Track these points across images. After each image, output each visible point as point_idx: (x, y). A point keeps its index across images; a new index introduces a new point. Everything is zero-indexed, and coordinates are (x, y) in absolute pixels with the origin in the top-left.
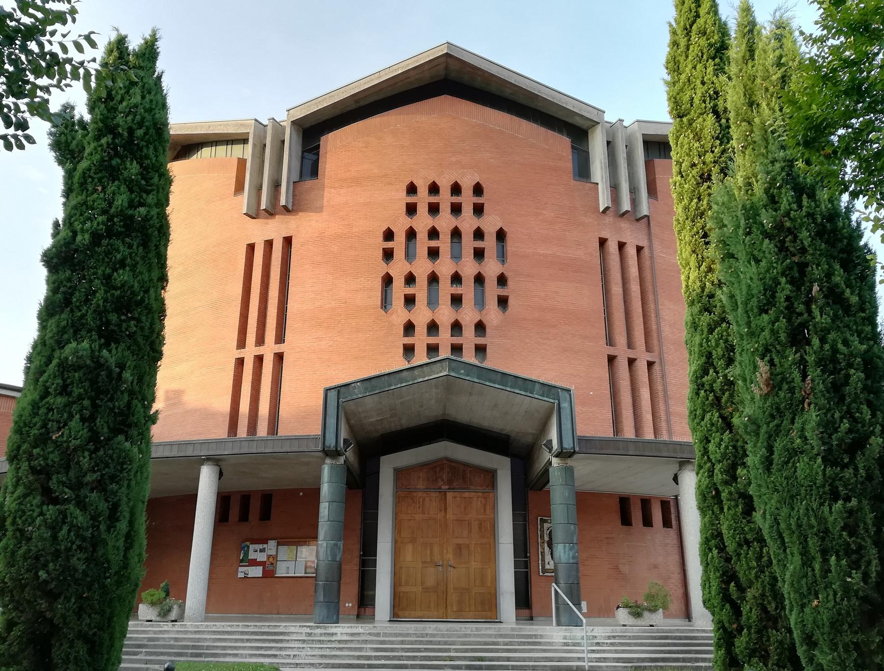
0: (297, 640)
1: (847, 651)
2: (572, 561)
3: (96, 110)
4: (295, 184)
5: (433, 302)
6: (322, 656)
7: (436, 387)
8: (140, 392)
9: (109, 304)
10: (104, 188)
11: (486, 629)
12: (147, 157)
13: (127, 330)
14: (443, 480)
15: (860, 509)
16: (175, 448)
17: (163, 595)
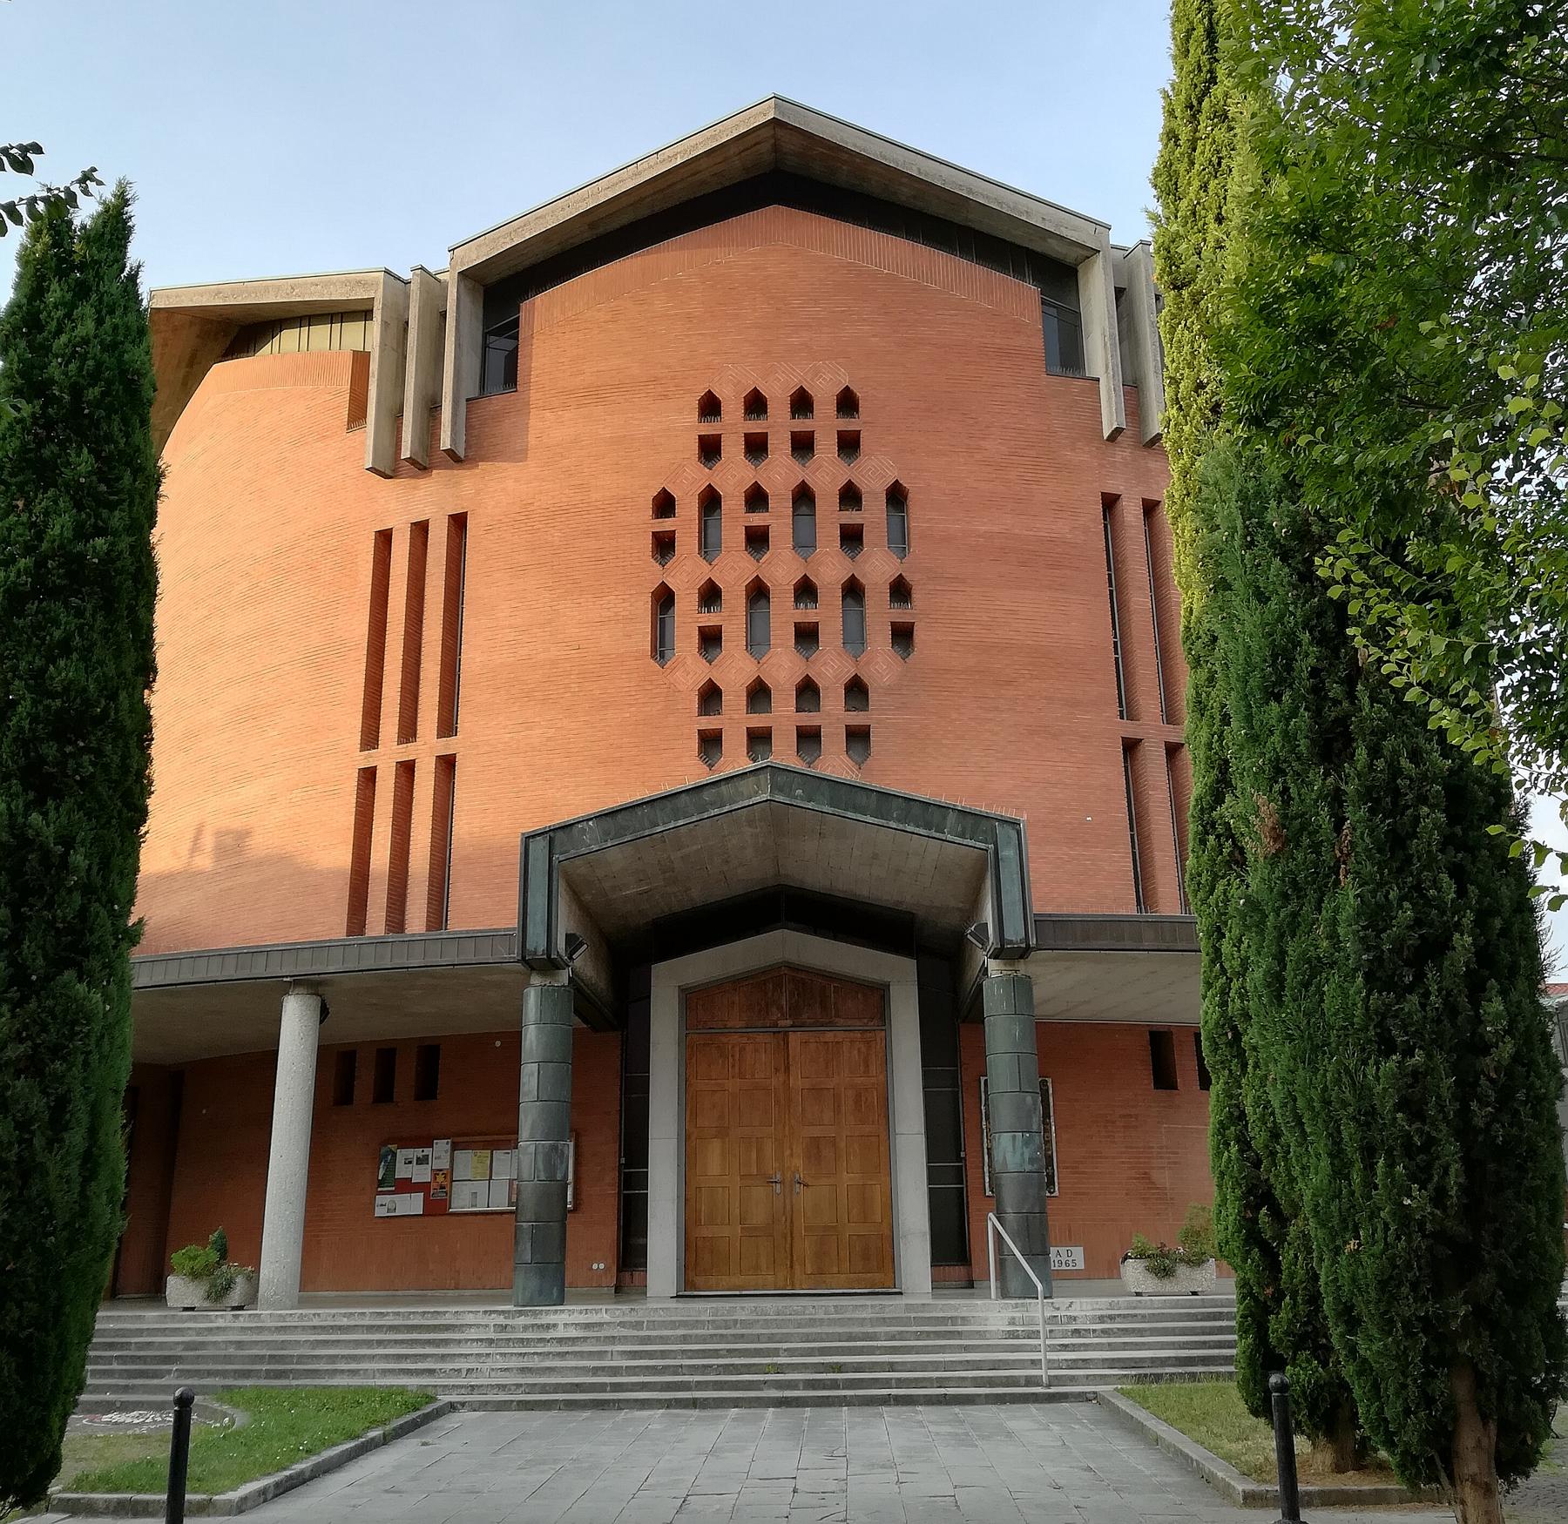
0: (477, 1340)
1: (1409, 1334)
2: (1028, 1167)
3: (11, 352)
4: (470, 405)
5: (756, 642)
6: (523, 1370)
7: (751, 823)
8: (104, 888)
9: (41, 726)
10: (28, 507)
12: (109, 438)
13: (76, 772)
14: (780, 1008)
15: (1430, 1071)
16: (231, 961)
17: (214, 1256)
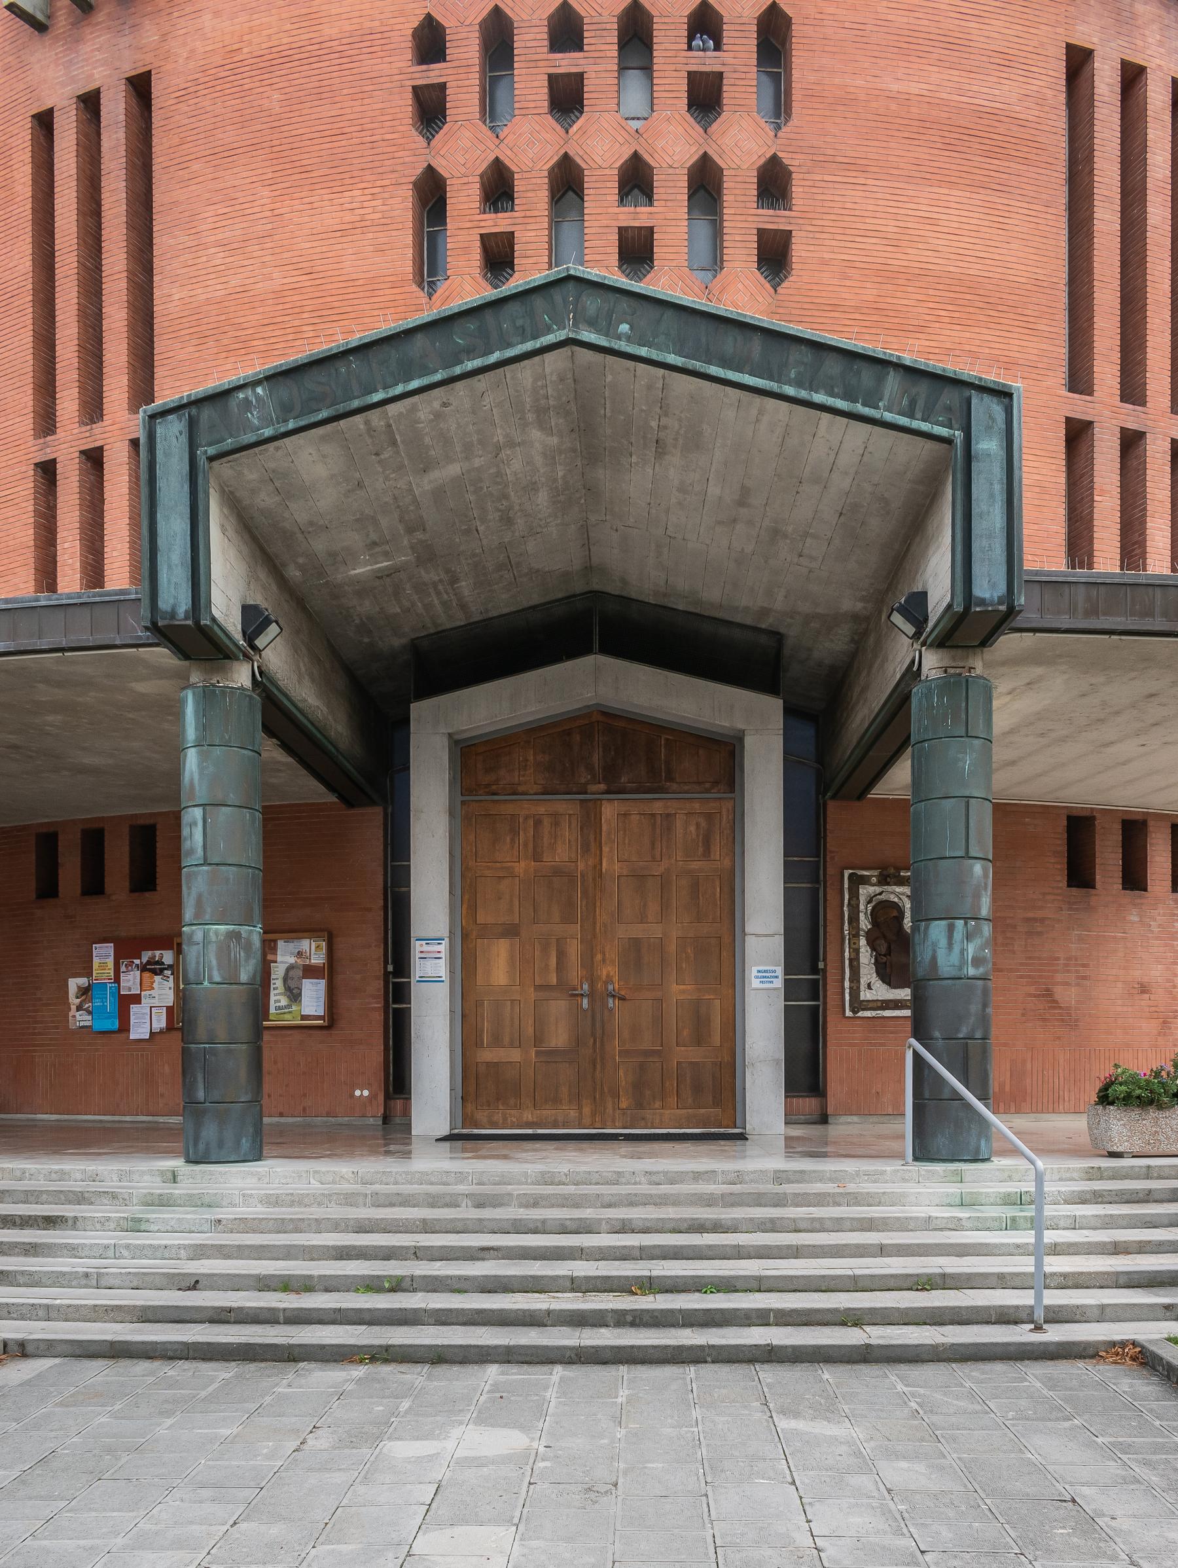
11: (697, 1176)
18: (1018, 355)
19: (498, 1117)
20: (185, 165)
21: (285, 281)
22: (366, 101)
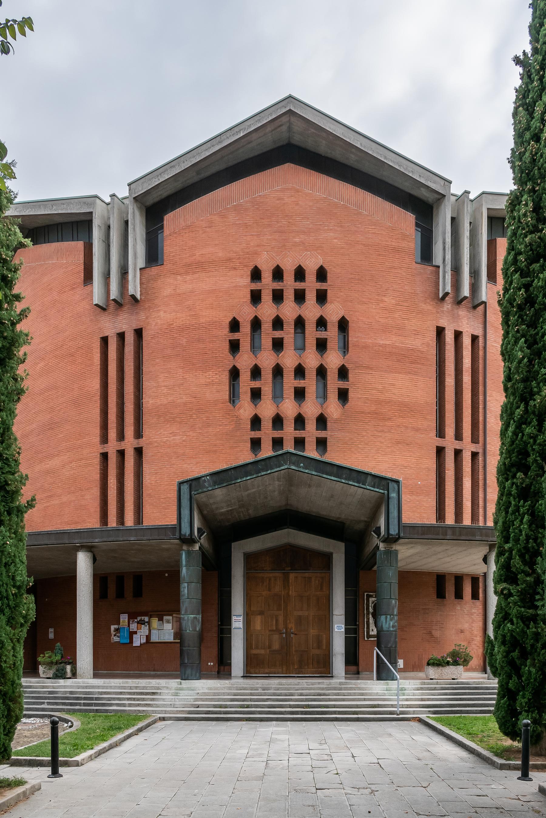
7: (279, 480)
11: (319, 683)
18: (421, 427)
19: (257, 671)
20: (154, 359)
21: (187, 400)
22: (214, 344)
